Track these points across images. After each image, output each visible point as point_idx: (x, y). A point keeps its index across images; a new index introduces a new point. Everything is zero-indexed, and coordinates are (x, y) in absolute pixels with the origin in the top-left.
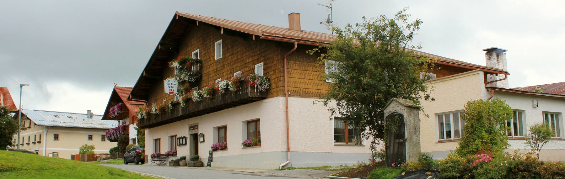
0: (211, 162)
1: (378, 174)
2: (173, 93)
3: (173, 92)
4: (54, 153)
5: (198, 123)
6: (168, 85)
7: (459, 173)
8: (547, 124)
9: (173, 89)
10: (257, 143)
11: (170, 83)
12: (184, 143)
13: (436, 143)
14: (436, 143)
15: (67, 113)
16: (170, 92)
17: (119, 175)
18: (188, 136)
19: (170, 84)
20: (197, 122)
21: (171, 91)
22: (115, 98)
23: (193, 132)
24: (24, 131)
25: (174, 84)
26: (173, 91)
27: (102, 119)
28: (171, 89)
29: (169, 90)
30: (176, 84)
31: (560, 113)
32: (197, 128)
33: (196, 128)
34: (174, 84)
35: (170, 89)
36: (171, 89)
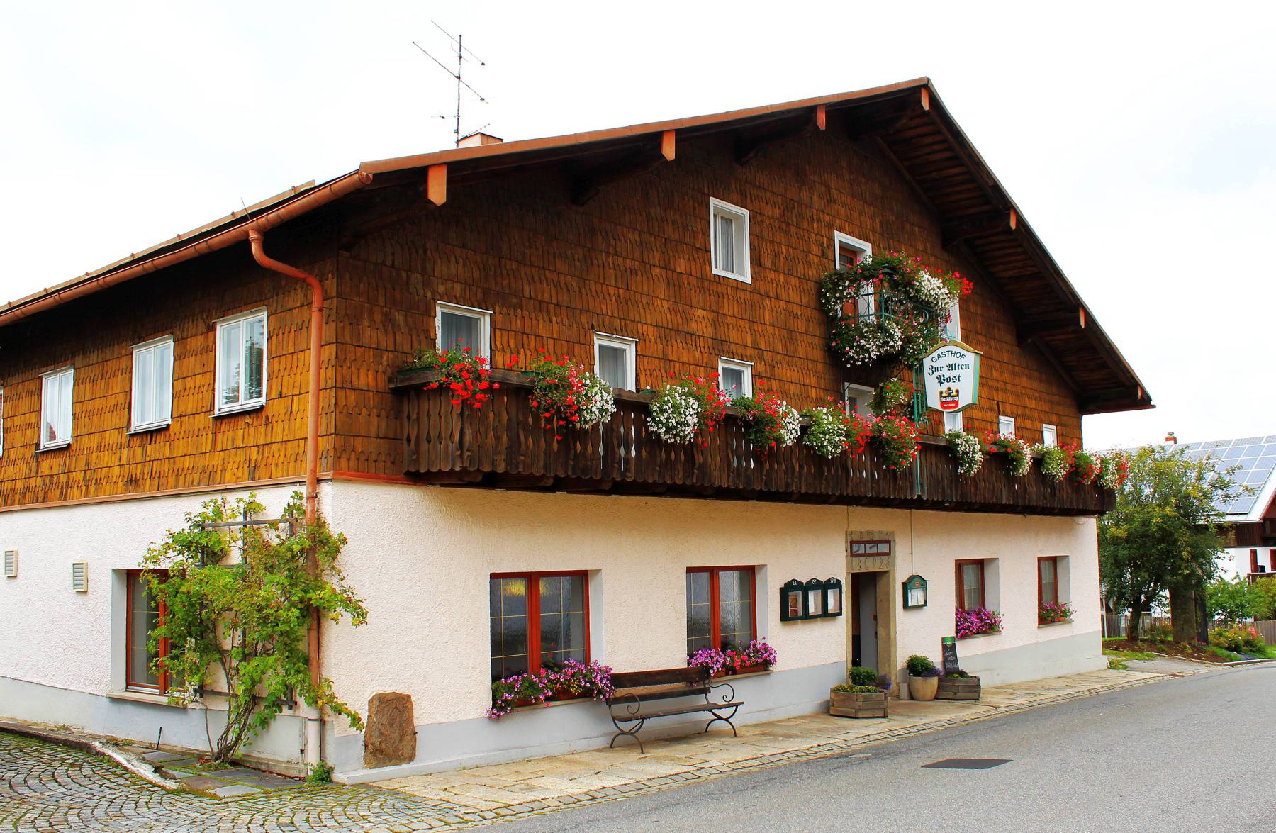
2: (956, 402)
3: (956, 398)
5: (893, 533)
6: (936, 374)
7: (203, 315)
8: (662, 758)
9: (954, 386)
10: (943, 638)
11: (943, 362)
13: (743, 703)
14: (743, 703)
16: (942, 403)
18: (843, 577)
19: (945, 369)
21: (949, 395)
22: (302, 549)
25: (960, 367)
26: (958, 396)
28: (949, 389)
29: (941, 393)
30: (967, 366)
31: (992, 560)
32: (888, 554)
33: (883, 548)
34: (960, 367)
36: (949, 389)
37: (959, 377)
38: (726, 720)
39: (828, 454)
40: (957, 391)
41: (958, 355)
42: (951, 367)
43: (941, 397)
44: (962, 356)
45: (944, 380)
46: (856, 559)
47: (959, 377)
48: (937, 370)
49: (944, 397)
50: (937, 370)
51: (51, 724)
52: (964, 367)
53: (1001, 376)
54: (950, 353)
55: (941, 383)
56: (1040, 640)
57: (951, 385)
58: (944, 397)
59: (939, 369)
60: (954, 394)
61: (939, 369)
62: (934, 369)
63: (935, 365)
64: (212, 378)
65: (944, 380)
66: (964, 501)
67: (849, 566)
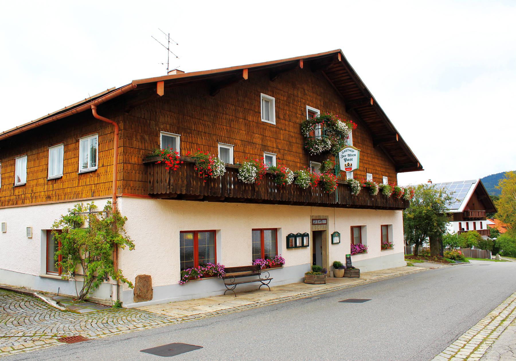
0: (459, 231)
1: (424, 215)
2: (351, 168)
3: (351, 167)
4: (234, 150)
5: (328, 216)
6: (344, 158)
9: (350, 162)
12: (298, 244)
15: (42, 205)
16: (346, 169)
17: (203, 299)
19: (347, 156)
20: (327, 215)
21: (348, 166)
23: (318, 227)
24: (85, 302)
25: (352, 155)
26: (351, 166)
27: (420, 168)
28: (348, 163)
29: (345, 165)
30: (355, 155)
34: (352, 155)
35: (347, 163)
36: (348, 163)
37: (352, 159)
40: (351, 164)
43: (345, 166)
44: (353, 151)
45: (346, 160)
46: (314, 226)
47: (352, 159)
49: (346, 166)
52: (354, 155)
55: (345, 161)
58: (346, 166)
60: (350, 165)
62: (343, 156)
63: (343, 155)
65: (346, 160)
67: (312, 228)
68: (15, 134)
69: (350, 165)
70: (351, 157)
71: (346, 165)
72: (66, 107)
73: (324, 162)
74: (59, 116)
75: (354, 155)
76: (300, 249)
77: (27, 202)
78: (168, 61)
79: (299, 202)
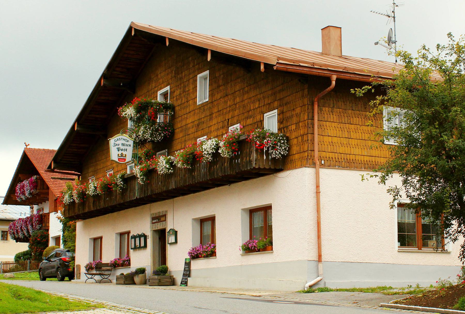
2: (125, 159)
3: (125, 158)
5: (166, 211)
6: (117, 147)
9: (124, 153)
11: (119, 142)
16: (119, 159)
19: (120, 145)
21: (122, 156)
25: (127, 145)
28: (122, 154)
29: (118, 155)
30: (130, 145)
32: (165, 220)
34: (127, 145)
35: (120, 152)
36: (122, 154)
37: (127, 149)
38: (89, 278)
39: (426, 142)
40: (125, 155)
41: (126, 140)
42: (123, 145)
43: (118, 156)
44: (128, 141)
45: (120, 149)
46: (154, 224)
47: (127, 149)
48: (117, 145)
49: (120, 157)
50: (117, 145)
51: (311, 51)
52: (128, 146)
53: (50, 169)
54: (123, 139)
55: (119, 151)
56: (243, 264)
57: (123, 152)
58: (120, 157)
59: (118, 145)
60: (124, 156)
61: (118, 145)
62: (115, 145)
63: (116, 143)
64: (317, 302)
65: (120, 149)
66: (153, 194)
67: (152, 227)
68: (295, 72)
69: (124, 156)
70: (125, 147)
71: (120, 155)
72: (431, 286)
73: (172, 168)
74: (160, 246)
75: (128, 146)
76: (141, 250)
77: (337, 167)
78: (314, 188)
79: (97, 210)
